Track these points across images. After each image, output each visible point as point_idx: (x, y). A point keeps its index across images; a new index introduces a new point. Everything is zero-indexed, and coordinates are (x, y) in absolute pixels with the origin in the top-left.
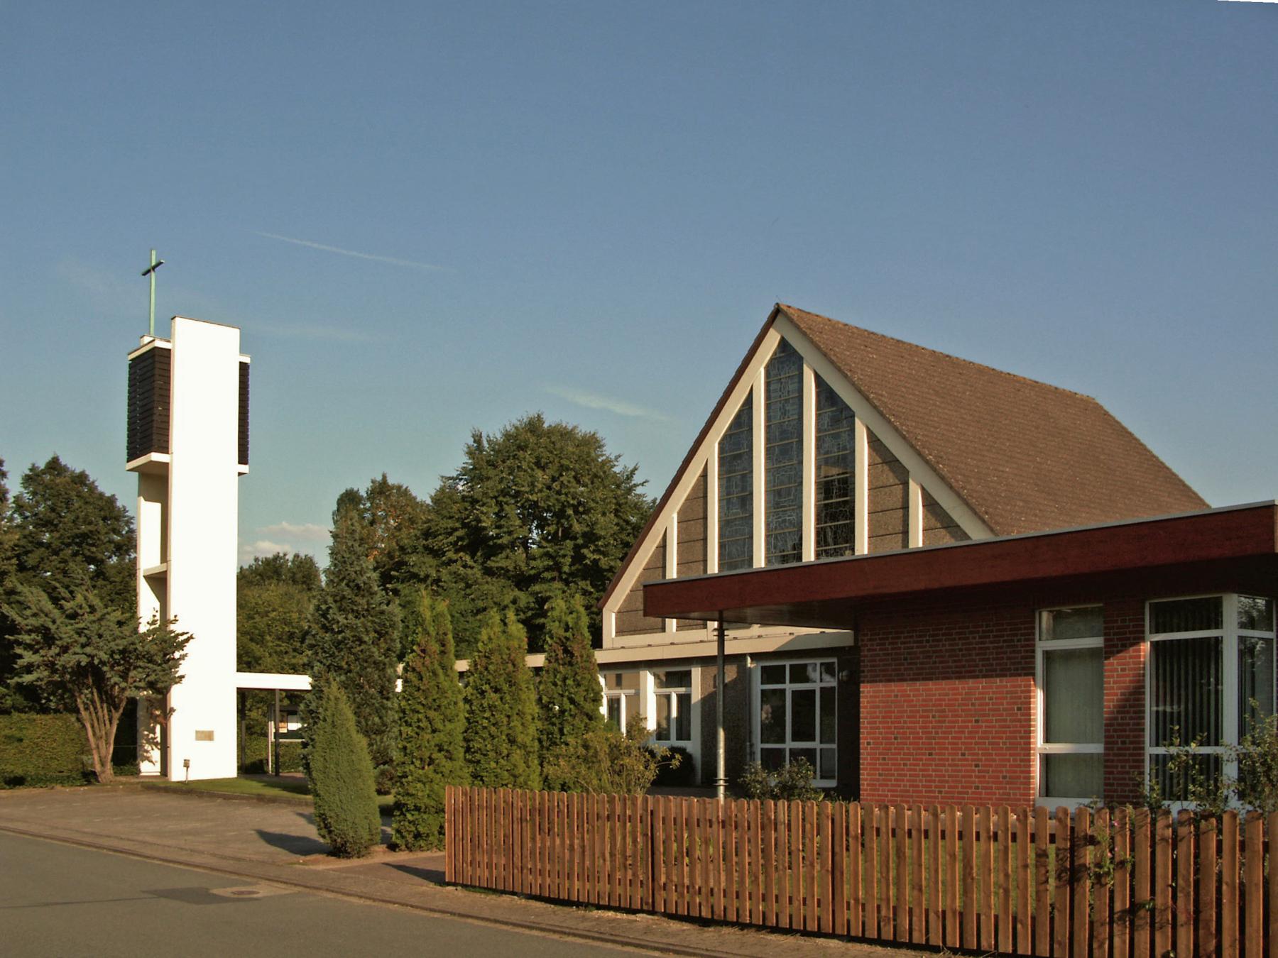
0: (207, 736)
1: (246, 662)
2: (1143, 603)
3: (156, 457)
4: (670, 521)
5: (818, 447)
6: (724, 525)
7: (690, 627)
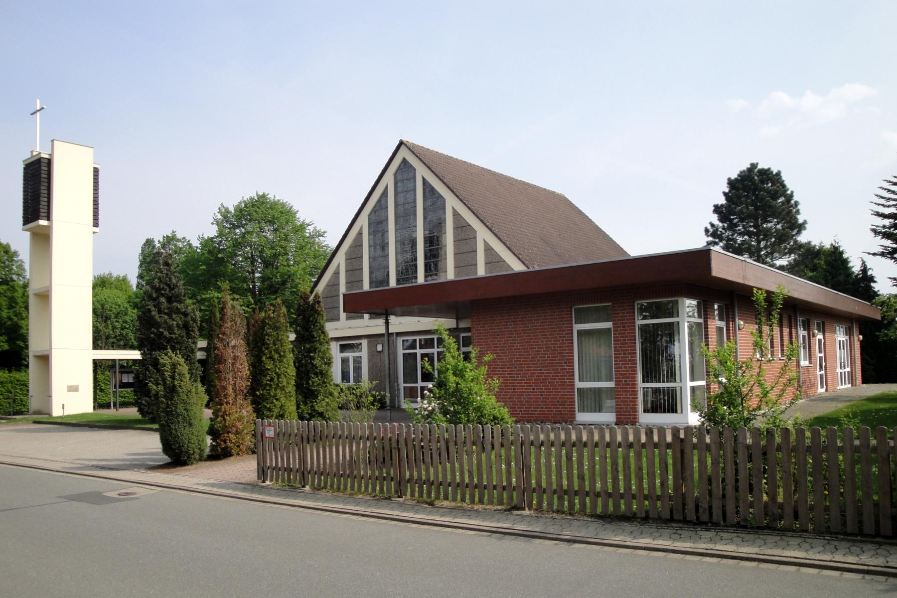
0: (73, 389)
1: (99, 341)
2: (634, 302)
3: (43, 222)
4: (340, 259)
5: (425, 218)
6: (372, 259)
7: (354, 318)
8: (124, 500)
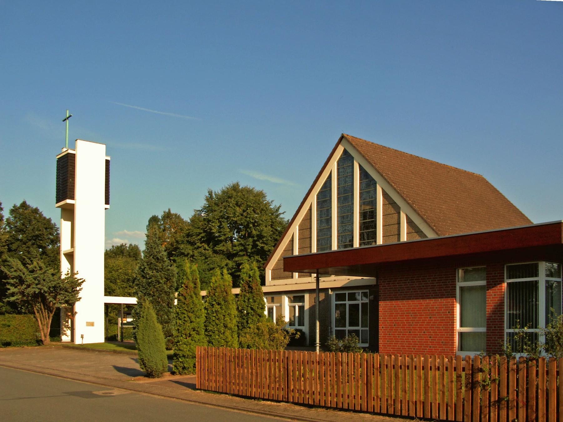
1: (109, 292)
3: (69, 201)
4: (295, 230)
5: (360, 197)
6: (319, 231)
8: (105, 396)
